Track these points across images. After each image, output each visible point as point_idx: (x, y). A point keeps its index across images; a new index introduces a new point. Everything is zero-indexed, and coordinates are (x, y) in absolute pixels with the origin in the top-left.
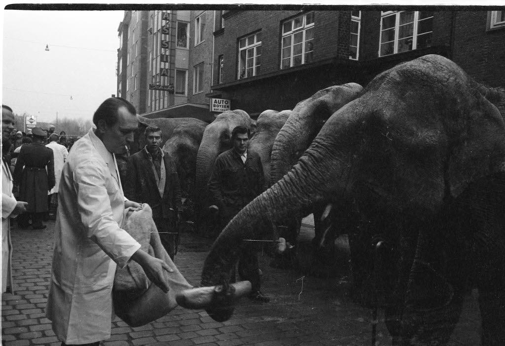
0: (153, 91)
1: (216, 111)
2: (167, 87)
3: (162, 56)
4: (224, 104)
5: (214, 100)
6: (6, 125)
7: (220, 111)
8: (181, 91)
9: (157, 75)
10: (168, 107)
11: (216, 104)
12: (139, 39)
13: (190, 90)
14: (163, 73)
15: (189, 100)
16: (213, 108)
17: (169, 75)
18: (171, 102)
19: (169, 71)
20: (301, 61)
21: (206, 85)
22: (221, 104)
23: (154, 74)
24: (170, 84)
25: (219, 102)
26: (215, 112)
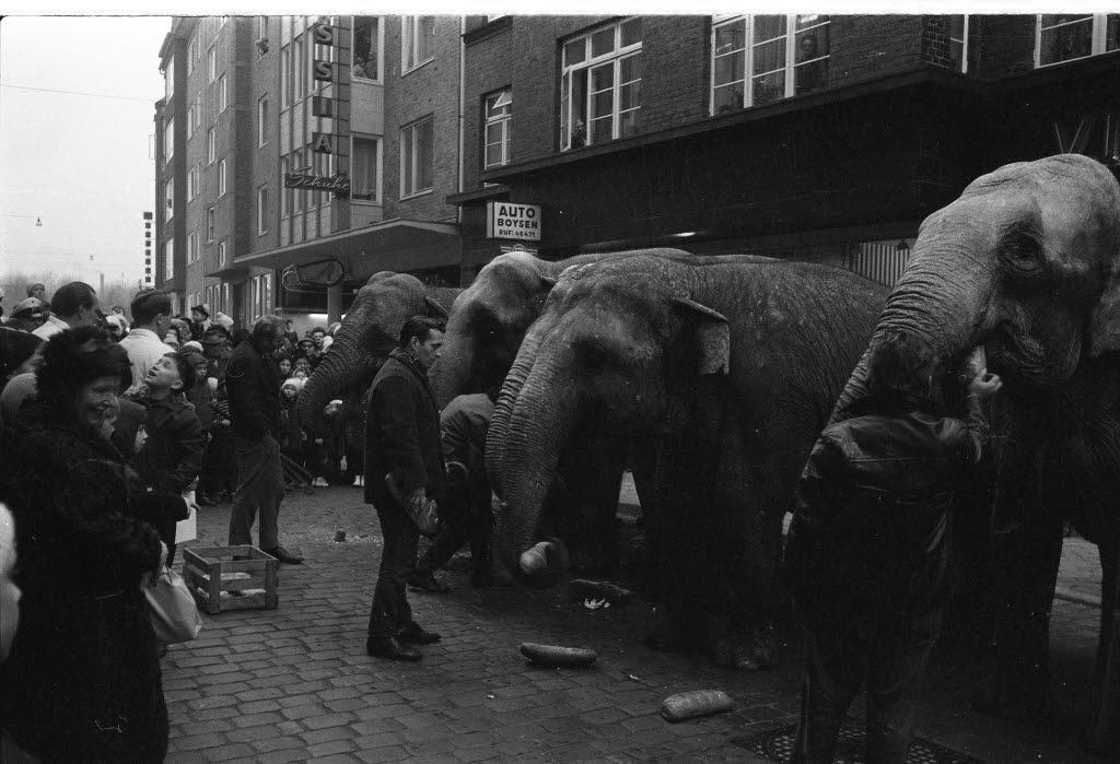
0: (296, 191)
1: (503, 236)
2: (332, 181)
3: (317, 100)
4: (525, 218)
5: (498, 205)
6: (1040, 18)
7: (515, 237)
8: (365, 192)
9: (294, 152)
10: (333, 233)
11: (503, 217)
12: (230, 68)
13: (391, 187)
14: (319, 145)
15: (388, 212)
16: (497, 228)
17: (334, 149)
18: (342, 222)
19: (335, 139)
20: (610, 130)
21: (443, 174)
22: (518, 218)
23: (285, 150)
24: (339, 174)
25: (513, 213)
26: (502, 239)
